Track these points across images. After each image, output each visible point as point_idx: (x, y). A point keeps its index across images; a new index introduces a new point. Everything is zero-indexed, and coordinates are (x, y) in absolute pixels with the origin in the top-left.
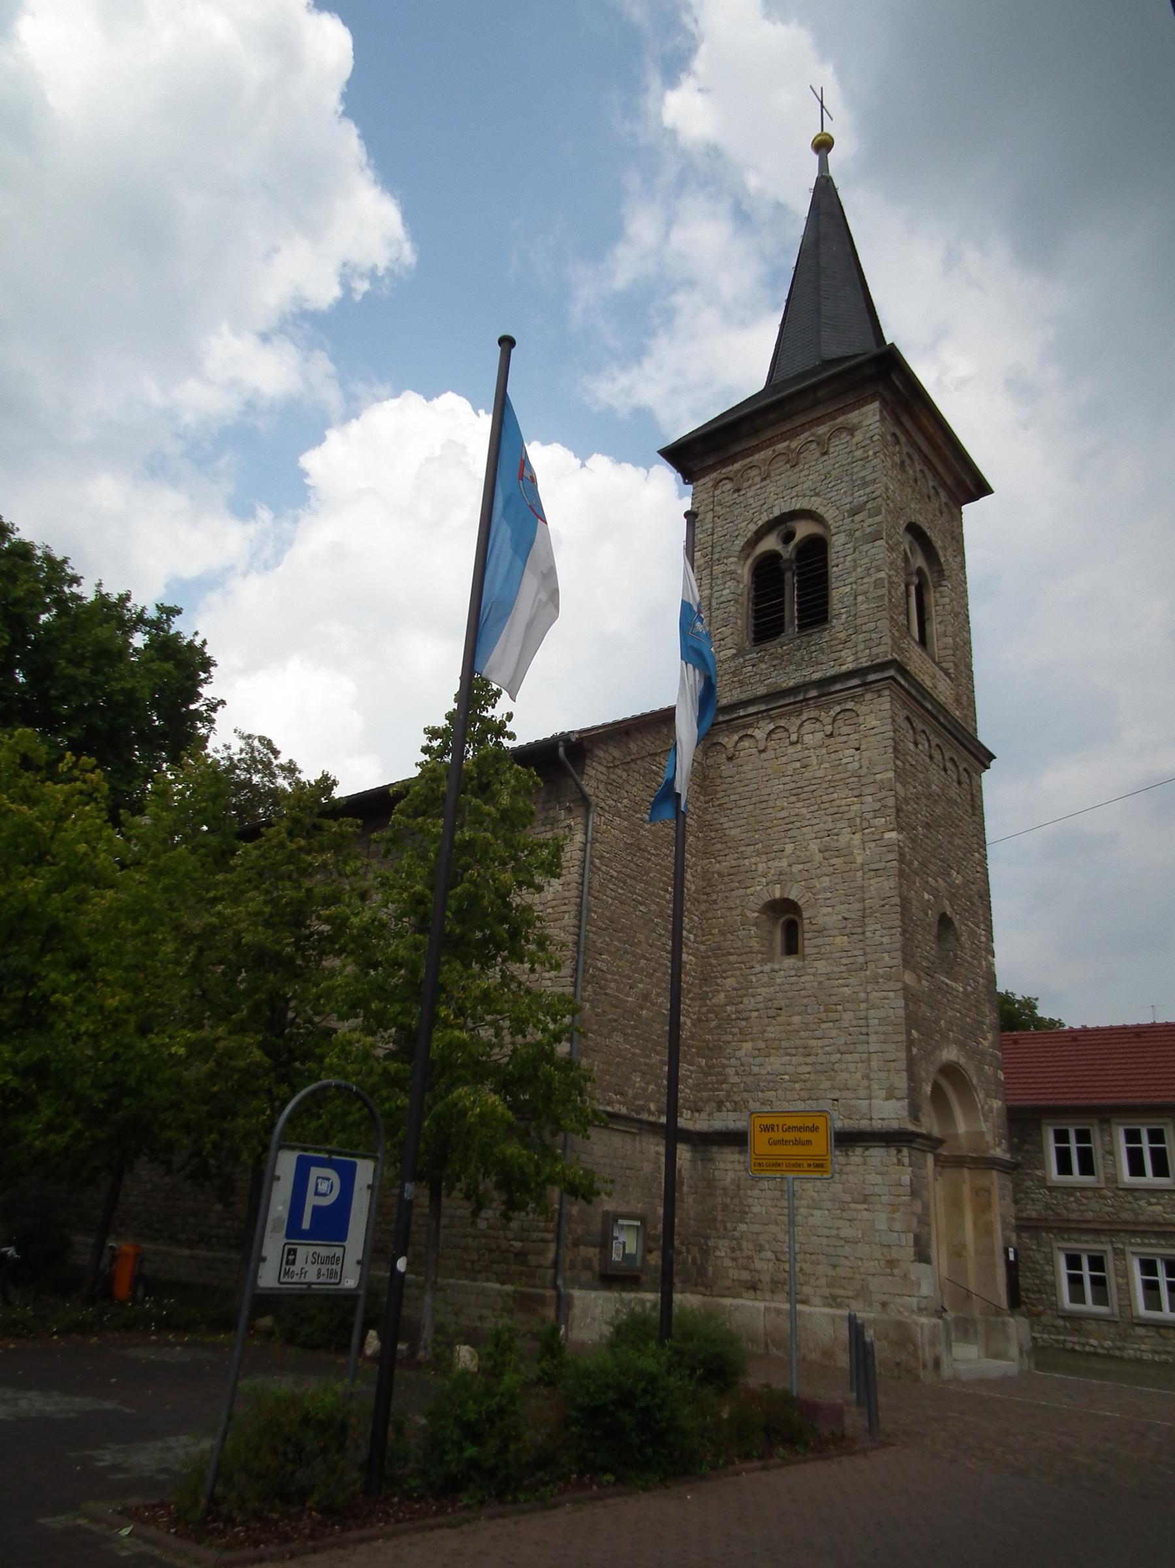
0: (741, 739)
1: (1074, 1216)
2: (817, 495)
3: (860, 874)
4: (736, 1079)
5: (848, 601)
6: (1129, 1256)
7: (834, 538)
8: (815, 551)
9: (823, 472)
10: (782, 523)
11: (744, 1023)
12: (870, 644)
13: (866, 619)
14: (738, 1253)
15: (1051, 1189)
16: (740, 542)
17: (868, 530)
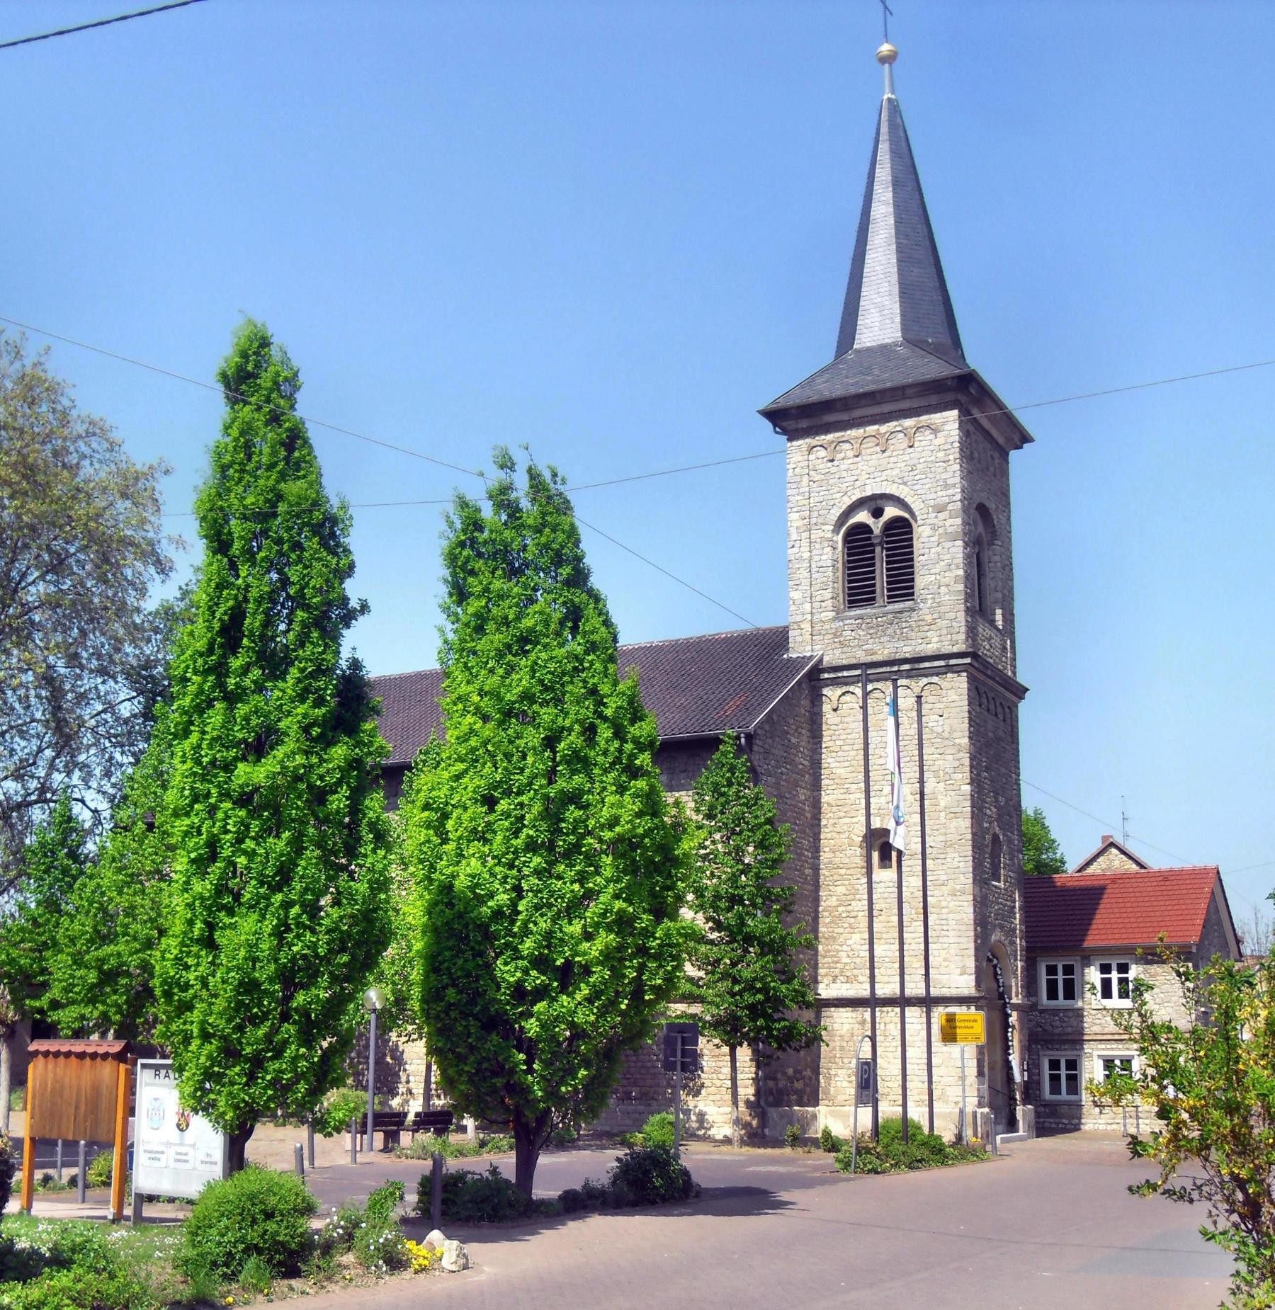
0: (843, 694)
1: (1057, 1031)
2: (905, 484)
3: (943, 814)
4: (848, 960)
5: (933, 588)
6: (1095, 1058)
7: (921, 529)
8: (901, 531)
9: (910, 463)
10: (875, 504)
11: (852, 920)
12: (951, 630)
13: (947, 609)
15: (1042, 1012)
16: (836, 513)
17: (950, 530)
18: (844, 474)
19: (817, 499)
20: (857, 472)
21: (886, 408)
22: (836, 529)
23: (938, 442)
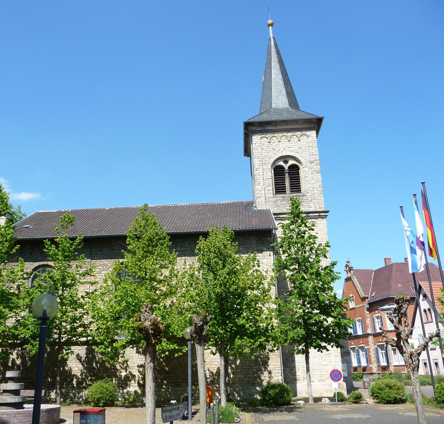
10: (285, 158)
12: (319, 203)
14: (292, 371)
16: (272, 161)
17: (316, 169)
18: (275, 147)
19: (265, 155)
20: (280, 147)
21: (290, 127)
22: (271, 167)
23: (309, 140)
